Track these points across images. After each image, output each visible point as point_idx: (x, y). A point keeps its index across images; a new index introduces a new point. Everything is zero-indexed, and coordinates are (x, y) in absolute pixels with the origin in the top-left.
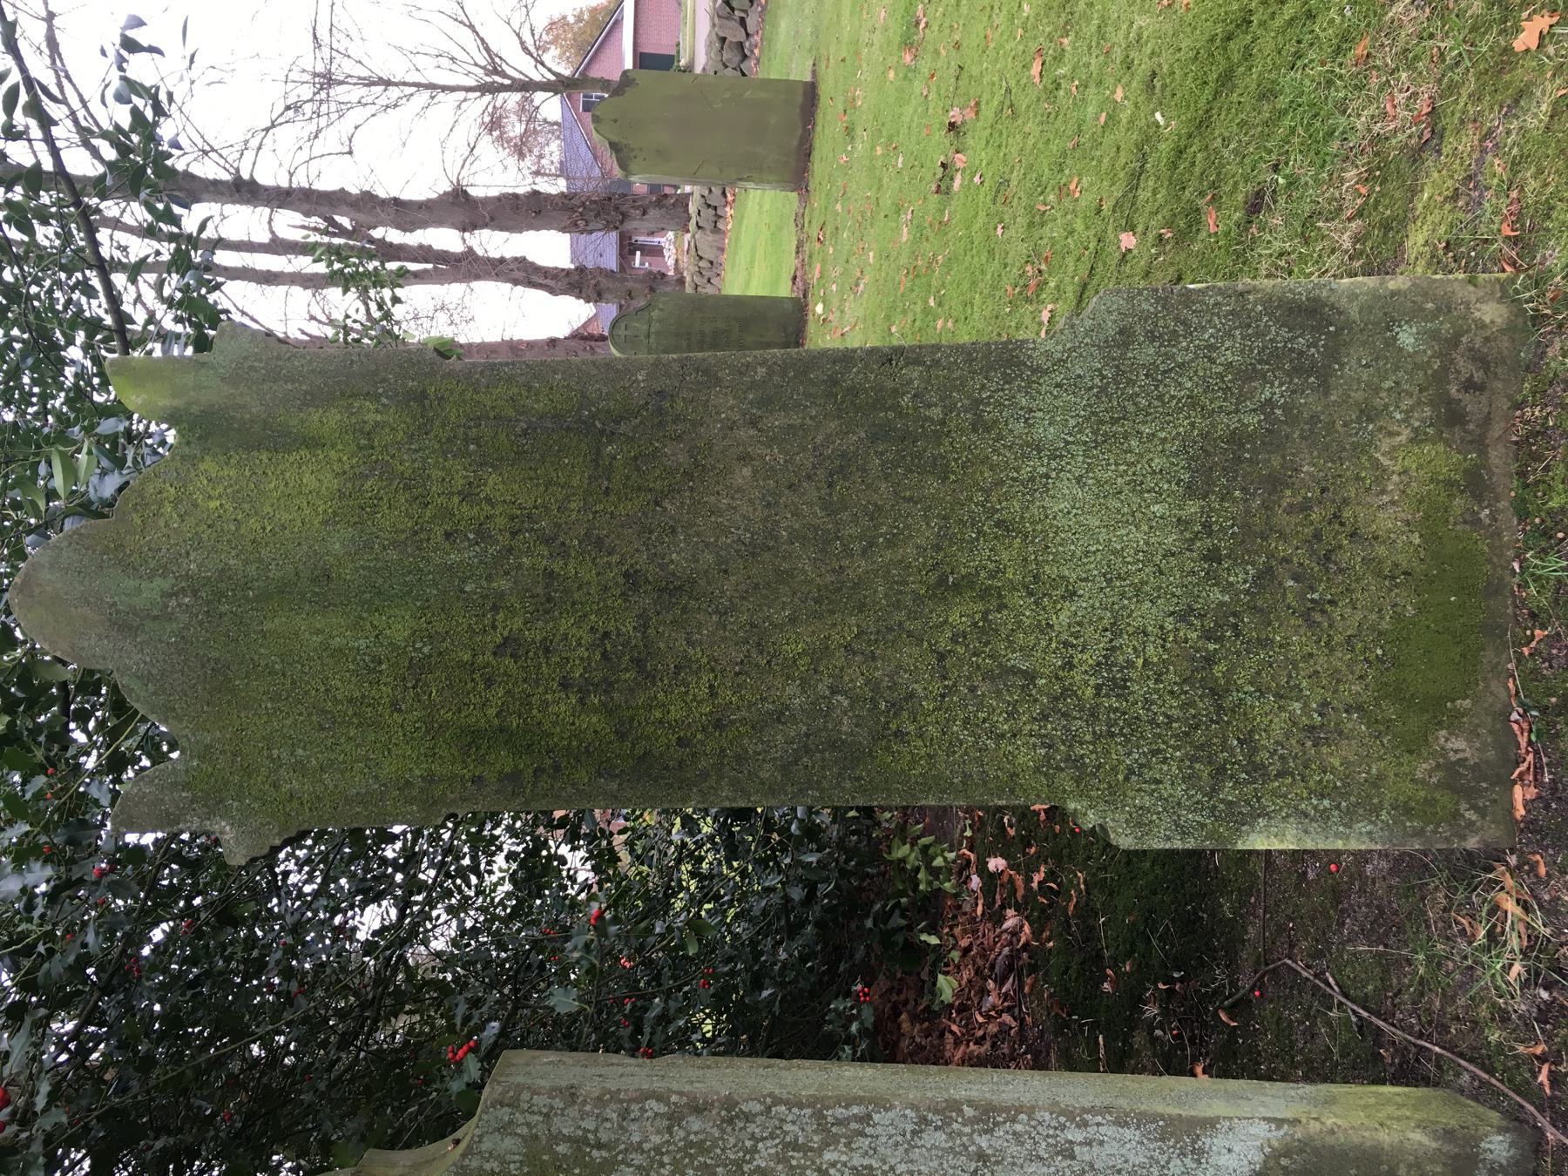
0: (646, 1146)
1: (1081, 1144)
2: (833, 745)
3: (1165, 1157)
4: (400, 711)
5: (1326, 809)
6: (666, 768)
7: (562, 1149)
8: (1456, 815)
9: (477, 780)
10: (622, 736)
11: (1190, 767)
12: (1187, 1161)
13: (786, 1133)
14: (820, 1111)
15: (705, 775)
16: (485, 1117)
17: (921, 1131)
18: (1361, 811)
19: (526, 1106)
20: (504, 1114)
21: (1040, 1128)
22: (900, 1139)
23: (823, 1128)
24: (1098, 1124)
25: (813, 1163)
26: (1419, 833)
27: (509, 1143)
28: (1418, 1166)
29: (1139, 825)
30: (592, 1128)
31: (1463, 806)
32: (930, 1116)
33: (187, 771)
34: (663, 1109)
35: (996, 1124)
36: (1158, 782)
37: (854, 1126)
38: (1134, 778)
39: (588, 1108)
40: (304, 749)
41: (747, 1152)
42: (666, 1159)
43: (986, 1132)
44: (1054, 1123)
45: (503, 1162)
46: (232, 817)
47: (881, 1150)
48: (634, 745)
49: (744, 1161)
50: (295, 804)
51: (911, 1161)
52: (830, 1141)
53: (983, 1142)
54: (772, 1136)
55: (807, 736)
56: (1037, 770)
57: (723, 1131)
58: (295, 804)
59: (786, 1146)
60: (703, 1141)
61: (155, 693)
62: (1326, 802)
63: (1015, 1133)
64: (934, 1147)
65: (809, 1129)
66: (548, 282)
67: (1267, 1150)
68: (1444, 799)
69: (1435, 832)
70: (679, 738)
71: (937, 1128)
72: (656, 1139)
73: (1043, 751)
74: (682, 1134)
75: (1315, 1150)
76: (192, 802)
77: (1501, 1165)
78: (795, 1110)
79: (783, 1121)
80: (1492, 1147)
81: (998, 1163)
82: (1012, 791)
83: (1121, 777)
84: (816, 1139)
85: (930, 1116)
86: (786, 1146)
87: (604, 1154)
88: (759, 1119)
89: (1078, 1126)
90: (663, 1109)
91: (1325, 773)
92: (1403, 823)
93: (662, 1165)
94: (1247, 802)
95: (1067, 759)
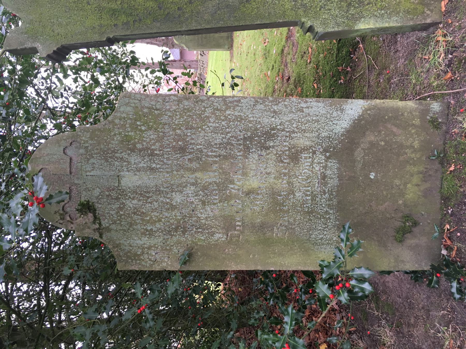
0: (171, 110)
1: (305, 108)
2: (227, 6)
3: (332, 111)
4: (89, 4)
5: (383, 14)
6: (175, 18)
7: (145, 110)
8: (424, 12)
9: (115, 25)
10: (160, 8)
11: (340, 4)
12: (339, 112)
13: (214, 106)
14: (225, 99)
15: (187, 19)
16: (121, 101)
17: (256, 105)
18: (394, 14)
19: (133, 98)
20: (127, 100)
21: (293, 103)
22: (249, 107)
23: (226, 104)
24: (311, 102)
25: (223, 114)
26: (412, 19)
27: (129, 109)
28: (411, 113)
29: (324, 24)
30: (154, 104)
31: (426, 10)
32: (259, 100)
33: (26, 28)
34: (176, 98)
35: (279, 102)
36: (330, 10)
37: (235, 103)
38: (322, 9)
39: (153, 98)
40: (61, 18)
41: (202, 111)
42: (178, 114)
43: (276, 105)
44: (297, 102)
45: (128, 114)
46: (41, 42)
47: (244, 110)
48: (164, 11)
49: (202, 114)
50: (60, 36)
51: (253, 114)
52: (228, 108)
53: (275, 108)
54: (210, 107)
55: (219, 4)
56: (292, 9)
57: (195, 105)
58: (60, 36)
59: (214, 109)
60: (189, 108)
61: (14, 4)
62: (383, 12)
63: (285, 105)
64: (260, 109)
65: (221, 104)
66: (157, 43)
67: (363, 109)
68: (420, 8)
69: (417, 18)
70: (178, 8)
71: (261, 104)
72: (174, 108)
73: (293, 3)
74: (182, 106)
75: (379, 109)
76: (28, 38)
77: (437, 112)
78: (217, 99)
79: (213, 102)
80: (434, 107)
81: (280, 114)
82: (284, 17)
83: (318, 9)
84: (223, 107)
85: (259, 100)
86: (214, 109)
87: (159, 112)
88: (206, 102)
89: (305, 102)
90: (176, 98)
91: (382, 2)
92: (407, 16)
93: (177, 115)
94: (358, 14)
95: (301, 5)
